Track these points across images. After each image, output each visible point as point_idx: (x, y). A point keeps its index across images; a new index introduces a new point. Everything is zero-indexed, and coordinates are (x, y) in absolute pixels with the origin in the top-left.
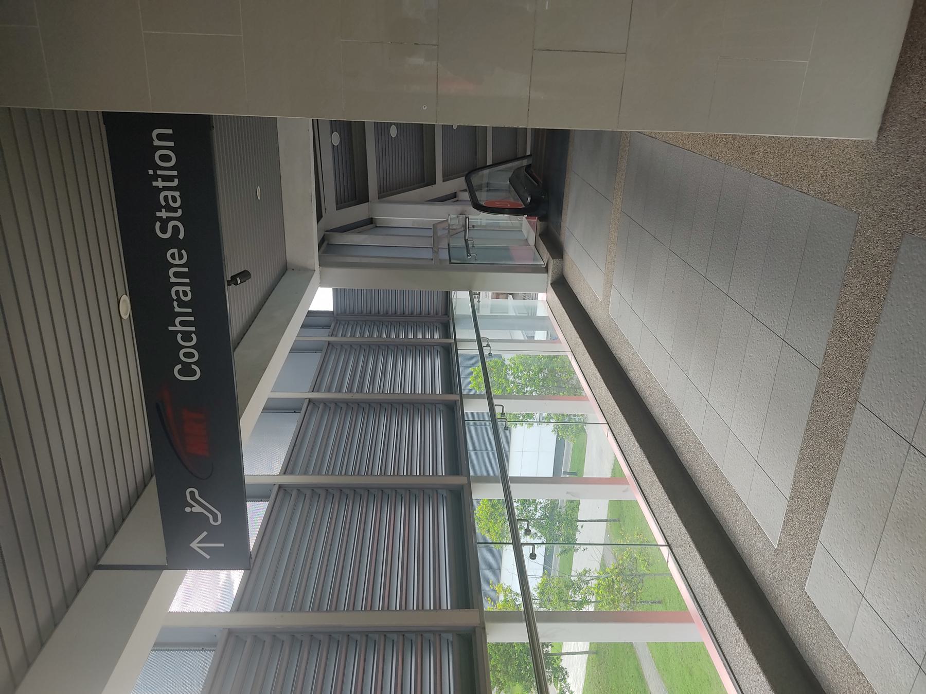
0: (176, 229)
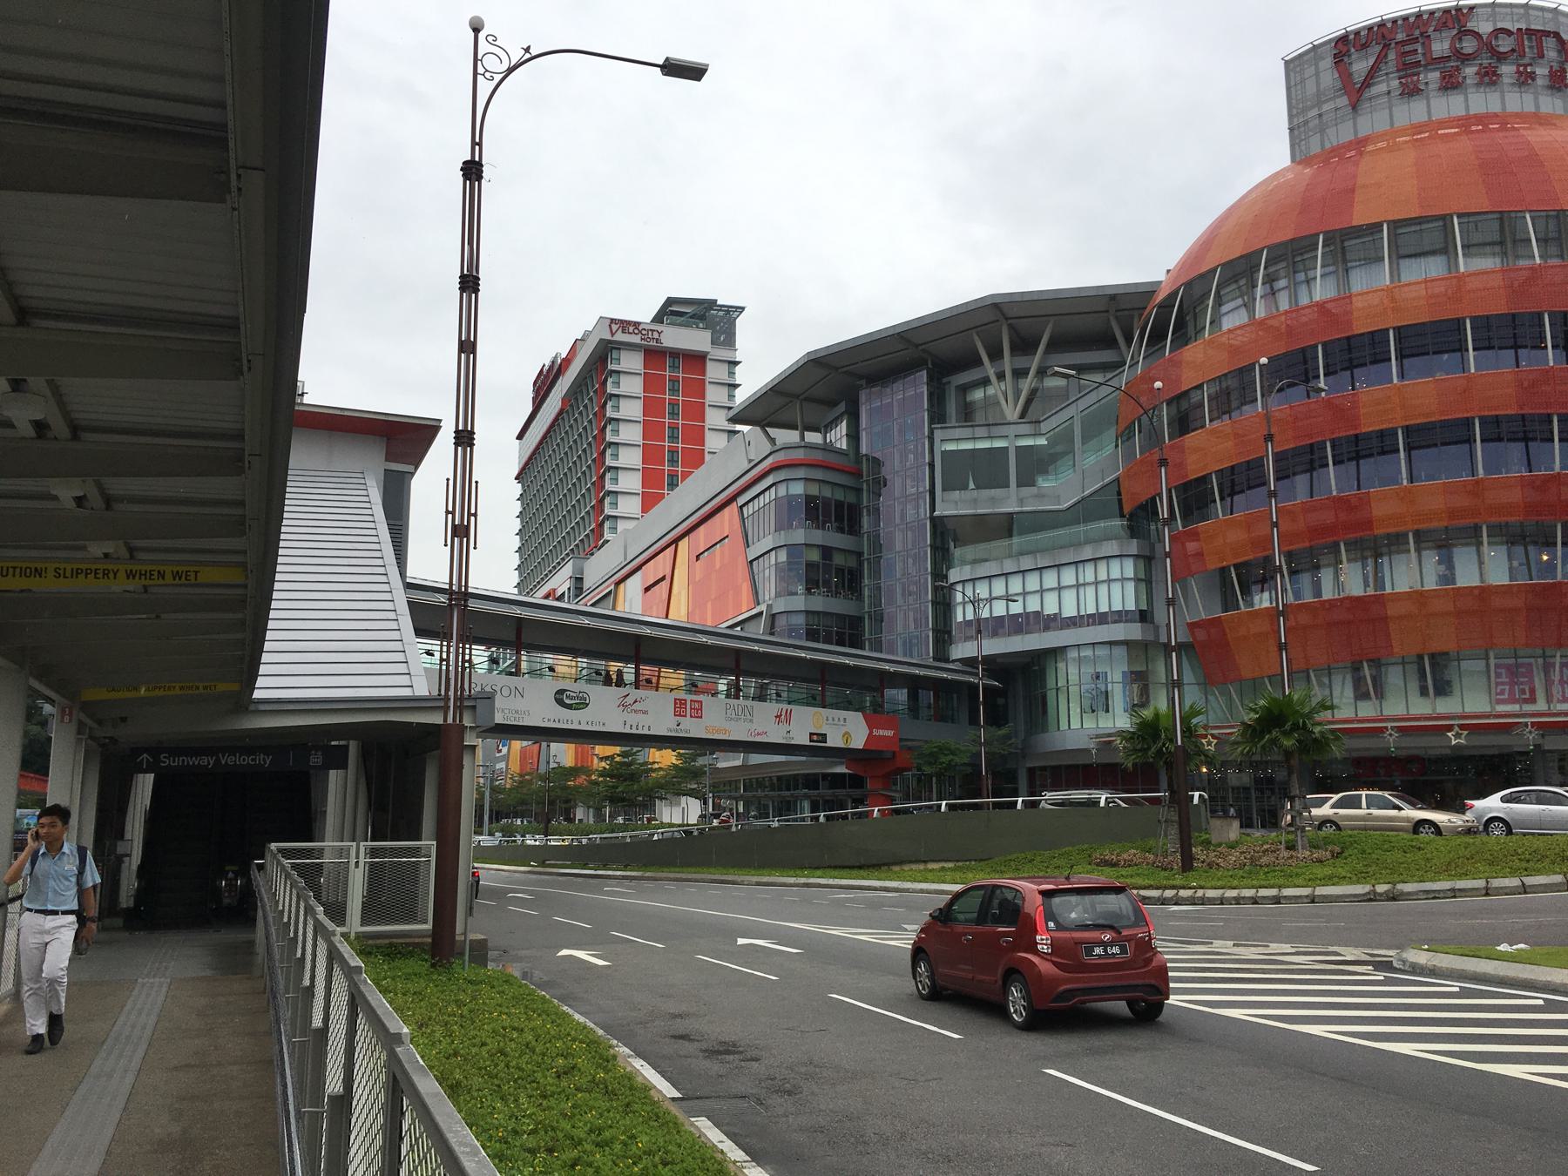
0: (165, 762)
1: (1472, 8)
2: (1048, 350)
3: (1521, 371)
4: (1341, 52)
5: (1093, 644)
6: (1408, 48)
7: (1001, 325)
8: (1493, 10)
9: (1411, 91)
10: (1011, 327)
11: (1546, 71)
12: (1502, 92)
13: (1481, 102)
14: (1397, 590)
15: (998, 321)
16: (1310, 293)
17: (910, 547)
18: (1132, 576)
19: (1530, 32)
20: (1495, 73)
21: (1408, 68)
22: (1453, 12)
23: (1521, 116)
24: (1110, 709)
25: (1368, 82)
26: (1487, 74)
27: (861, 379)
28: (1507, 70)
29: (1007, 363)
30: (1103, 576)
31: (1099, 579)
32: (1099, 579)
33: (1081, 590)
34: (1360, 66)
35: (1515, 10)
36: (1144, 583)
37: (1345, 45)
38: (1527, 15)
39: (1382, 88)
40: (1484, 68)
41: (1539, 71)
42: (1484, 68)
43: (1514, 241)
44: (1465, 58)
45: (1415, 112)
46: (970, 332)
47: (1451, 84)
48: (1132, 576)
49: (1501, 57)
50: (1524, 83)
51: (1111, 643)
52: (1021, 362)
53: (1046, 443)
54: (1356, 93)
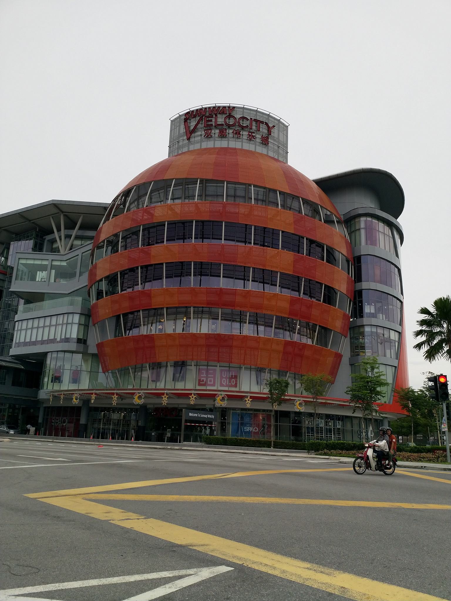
1: (234, 108)
2: (81, 228)
3: (185, 244)
4: (187, 118)
5: (57, 351)
6: (210, 119)
7: (60, 215)
8: (256, 113)
9: (208, 136)
10: (65, 215)
11: (260, 137)
12: (242, 142)
13: (223, 144)
14: (202, 332)
15: (59, 213)
16: (351, 229)
17: (5, 308)
18: (83, 323)
19: (256, 120)
20: (239, 134)
21: (208, 128)
22: (227, 108)
23: (261, 154)
24: (238, 385)
25: (194, 131)
26: (236, 133)
27: (13, 234)
28: (245, 133)
29: (63, 232)
30: (70, 321)
31: (69, 322)
32: (69, 322)
33: (57, 327)
34: (193, 123)
35: (251, 112)
36: (83, 327)
37: (189, 116)
38: (256, 115)
39: (199, 133)
40: (236, 131)
41: (257, 136)
42: (236, 131)
43: (205, 196)
44: (229, 126)
45: (209, 144)
46: (49, 217)
47: (223, 135)
48: (83, 323)
49: (243, 128)
50: (250, 140)
51: (65, 351)
52: (69, 232)
53: (66, 264)
54: (190, 133)
